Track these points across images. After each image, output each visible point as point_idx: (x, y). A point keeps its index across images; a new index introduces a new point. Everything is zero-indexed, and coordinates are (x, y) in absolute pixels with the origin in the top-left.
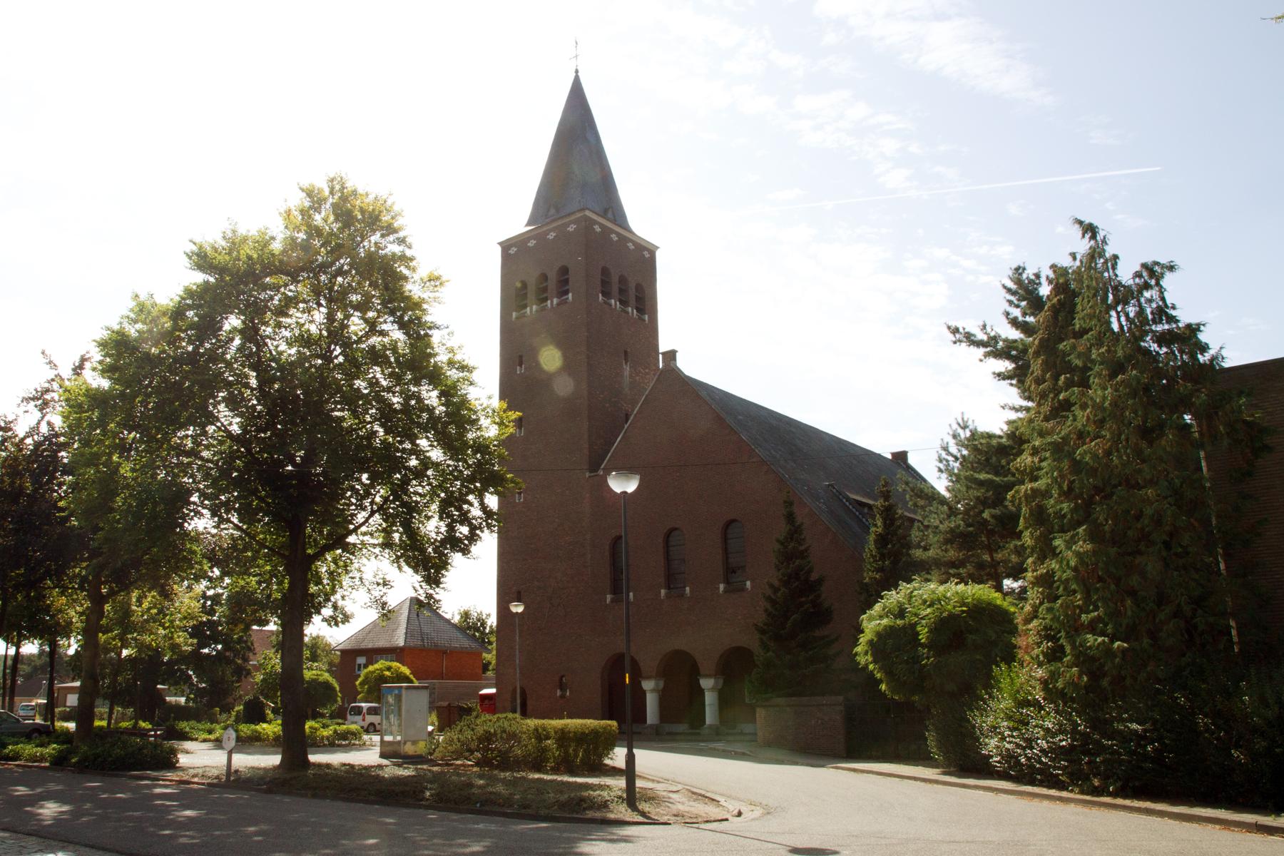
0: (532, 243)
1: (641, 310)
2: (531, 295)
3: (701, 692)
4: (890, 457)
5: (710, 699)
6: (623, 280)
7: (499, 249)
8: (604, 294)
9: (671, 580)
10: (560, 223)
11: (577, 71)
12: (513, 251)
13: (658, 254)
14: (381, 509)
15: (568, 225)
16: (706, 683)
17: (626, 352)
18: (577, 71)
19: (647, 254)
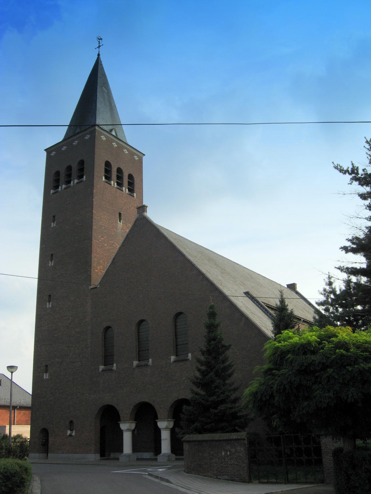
0: (64, 148)
1: (131, 190)
2: (62, 178)
3: (121, 433)
4: (286, 286)
5: (127, 438)
6: (119, 170)
7: (45, 153)
8: (106, 178)
9: (142, 355)
10: (80, 135)
11: (99, 55)
12: (53, 154)
13: (145, 159)
14: (254, 412)
15: (85, 136)
16: (124, 426)
17: (120, 214)
18: (99, 55)
19: (136, 158)
